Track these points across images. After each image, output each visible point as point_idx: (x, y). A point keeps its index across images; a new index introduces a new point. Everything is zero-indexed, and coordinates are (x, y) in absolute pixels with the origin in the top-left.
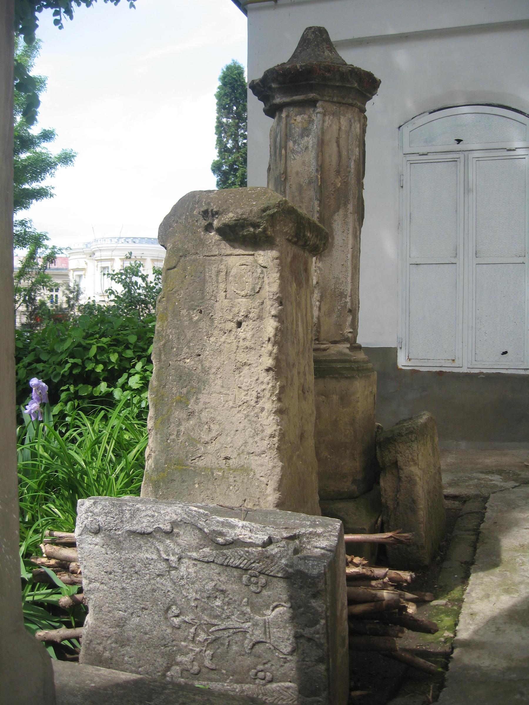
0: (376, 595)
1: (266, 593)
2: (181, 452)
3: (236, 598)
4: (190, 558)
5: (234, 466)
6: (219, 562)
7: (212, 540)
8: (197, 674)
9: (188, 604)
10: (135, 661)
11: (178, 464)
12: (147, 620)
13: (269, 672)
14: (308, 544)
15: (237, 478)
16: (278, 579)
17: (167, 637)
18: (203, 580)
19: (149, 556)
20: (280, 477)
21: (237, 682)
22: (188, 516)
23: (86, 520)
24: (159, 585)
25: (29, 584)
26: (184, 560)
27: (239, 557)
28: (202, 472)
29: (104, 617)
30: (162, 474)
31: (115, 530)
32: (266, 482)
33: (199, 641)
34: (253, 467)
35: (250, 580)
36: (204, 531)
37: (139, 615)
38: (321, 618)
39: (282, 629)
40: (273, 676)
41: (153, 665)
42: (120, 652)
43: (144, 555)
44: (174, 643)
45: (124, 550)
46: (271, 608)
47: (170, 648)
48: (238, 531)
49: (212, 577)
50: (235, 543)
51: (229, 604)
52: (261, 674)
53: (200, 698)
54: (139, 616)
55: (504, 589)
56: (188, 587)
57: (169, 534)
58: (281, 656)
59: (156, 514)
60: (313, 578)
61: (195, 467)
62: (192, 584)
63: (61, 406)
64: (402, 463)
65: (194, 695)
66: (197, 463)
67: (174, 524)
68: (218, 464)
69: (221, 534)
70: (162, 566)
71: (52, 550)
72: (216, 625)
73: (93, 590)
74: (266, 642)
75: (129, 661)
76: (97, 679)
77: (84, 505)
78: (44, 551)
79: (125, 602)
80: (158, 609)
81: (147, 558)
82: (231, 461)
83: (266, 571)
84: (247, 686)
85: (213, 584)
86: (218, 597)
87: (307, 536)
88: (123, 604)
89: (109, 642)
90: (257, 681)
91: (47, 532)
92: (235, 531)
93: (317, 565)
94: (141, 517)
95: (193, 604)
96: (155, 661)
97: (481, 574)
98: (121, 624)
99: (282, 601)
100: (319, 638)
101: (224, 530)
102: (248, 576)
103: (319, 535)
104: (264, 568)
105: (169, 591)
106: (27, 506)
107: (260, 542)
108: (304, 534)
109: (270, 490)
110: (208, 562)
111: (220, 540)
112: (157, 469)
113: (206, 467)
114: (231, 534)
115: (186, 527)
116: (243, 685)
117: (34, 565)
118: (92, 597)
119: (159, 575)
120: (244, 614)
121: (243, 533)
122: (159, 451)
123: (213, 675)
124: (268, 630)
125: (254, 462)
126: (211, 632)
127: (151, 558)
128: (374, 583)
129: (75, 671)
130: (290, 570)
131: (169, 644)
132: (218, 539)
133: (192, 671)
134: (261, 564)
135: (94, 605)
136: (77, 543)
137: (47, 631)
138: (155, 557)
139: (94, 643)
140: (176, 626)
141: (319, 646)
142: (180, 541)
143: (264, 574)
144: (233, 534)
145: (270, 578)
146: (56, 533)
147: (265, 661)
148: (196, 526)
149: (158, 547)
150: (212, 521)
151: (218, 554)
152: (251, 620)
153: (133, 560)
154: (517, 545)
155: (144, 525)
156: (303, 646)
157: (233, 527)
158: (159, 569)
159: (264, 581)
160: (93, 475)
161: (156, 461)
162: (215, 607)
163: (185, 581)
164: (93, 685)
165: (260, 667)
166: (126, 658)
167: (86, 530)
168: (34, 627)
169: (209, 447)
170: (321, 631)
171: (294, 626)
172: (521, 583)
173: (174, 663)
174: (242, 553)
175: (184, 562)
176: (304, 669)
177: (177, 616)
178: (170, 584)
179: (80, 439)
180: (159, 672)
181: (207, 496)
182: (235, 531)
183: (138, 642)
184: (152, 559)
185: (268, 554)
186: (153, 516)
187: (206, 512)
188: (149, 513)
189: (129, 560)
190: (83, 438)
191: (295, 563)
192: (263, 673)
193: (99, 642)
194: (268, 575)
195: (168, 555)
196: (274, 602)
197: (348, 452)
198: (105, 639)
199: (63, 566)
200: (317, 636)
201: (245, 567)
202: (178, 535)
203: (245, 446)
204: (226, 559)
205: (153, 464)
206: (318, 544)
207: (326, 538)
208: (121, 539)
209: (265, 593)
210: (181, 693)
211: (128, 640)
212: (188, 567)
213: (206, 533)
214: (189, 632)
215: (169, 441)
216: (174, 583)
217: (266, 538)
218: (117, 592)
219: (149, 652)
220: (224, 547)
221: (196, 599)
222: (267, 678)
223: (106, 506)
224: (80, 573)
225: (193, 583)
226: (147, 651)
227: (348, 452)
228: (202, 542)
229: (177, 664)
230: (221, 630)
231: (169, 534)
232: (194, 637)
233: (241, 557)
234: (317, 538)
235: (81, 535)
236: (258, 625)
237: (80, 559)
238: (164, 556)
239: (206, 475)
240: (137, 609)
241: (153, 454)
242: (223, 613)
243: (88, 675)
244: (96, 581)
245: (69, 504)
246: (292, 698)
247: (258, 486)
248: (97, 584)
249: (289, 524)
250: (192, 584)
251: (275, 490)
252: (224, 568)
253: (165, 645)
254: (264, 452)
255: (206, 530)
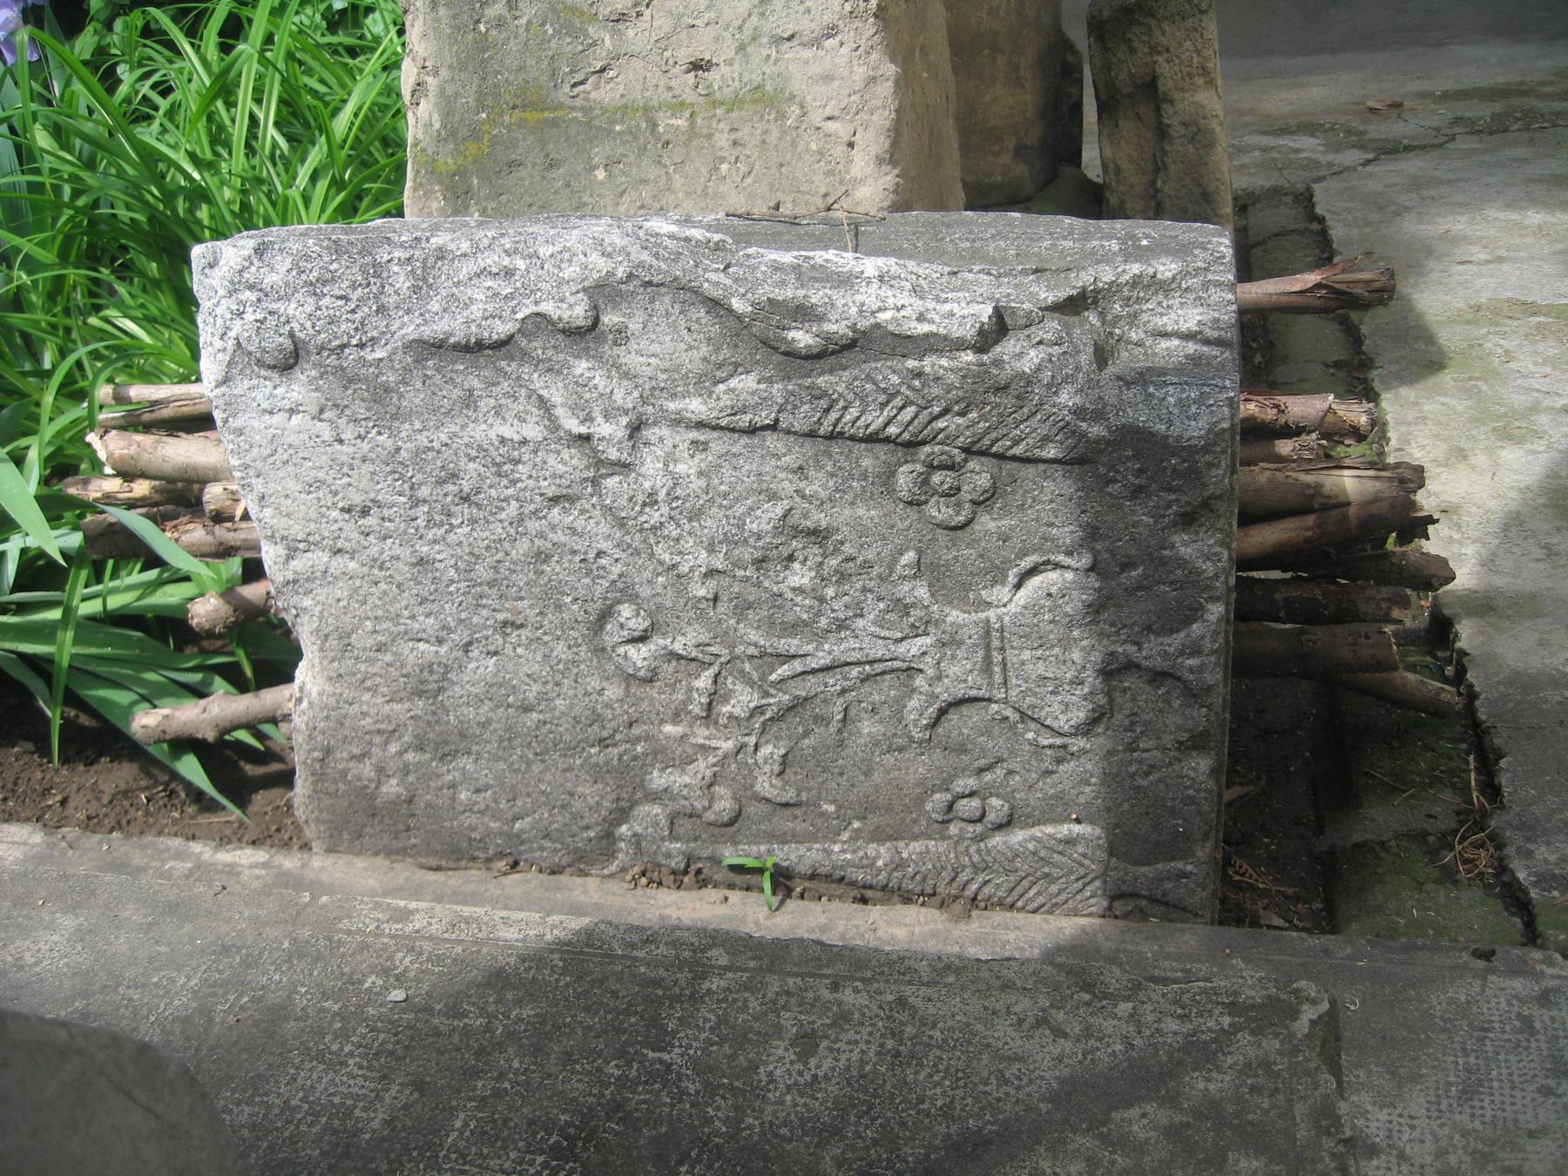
0: (1318, 486)
1: (992, 526)
2: (531, 62)
3: (870, 554)
4: (677, 421)
5: (726, 91)
6: (797, 427)
7: (765, 343)
8: (731, 823)
9: (682, 592)
10: (496, 801)
11: (524, 107)
12: (524, 663)
13: (998, 796)
14: (1131, 325)
15: (744, 133)
16: (1041, 467)
17: (609, 714)
18: (737, 500)
19: (508, 433)
20: (893, 116)
21: (878, 836)
22: (657, 256)
23: (238, 322)
24: (559, 537)
25: (80, 568)
26: (650, 434)
27: (882, 398)
28: (612, 122)
29: (363, 667)
30: (472, 147)
31: (361, 346)
32: (846, 138)
33: (731, 717)
34: (797, 86)
35: (926, 482)
36: (730, 311)
37: (492, 648)
38: (1212, 599)
39: (1056, 650)
40: (1012, 808)
41: (563, 807)
42: (439, 776)
43: (488, 430)
44: (636, 731)
45: (408, 417)
46: (1012, 579)
47: (622, 749)
48: (869, 296)
49: (774, 484)
50: (863, 343)
51: (843, 577)
52: (968, 806)
53: (863, 1000)
54: (496, 653)
55: (1494, 429)
56: (675, 534)
57: (584, 335)
58: (1046, 742)
59: (521, 264)
60: (1189, 452)
61: (586, 110)
62: (690, 520)
63: (96, 33)
64: (1171, 83)
65: (835, 987)
66: (593, 95)
67: (602, 293)
68: (670, 88)
69: (803, 313)
70: (567, 464)
71: (133, 451)
72: (794, 657)
73: (307, 580)
74: (989, 700)
75: (476, 803)
76: (403, 961)
77: (217, 266)
78: (102, 455)
79: (435, 607)
80: (563, 622)
81: (503, 441)
82: (713, 76)
83: (997, 440)
84: (916, 846)
85: (779, 511)
86: (800, 555)
87: (1126, 293)
88: (428, 615)
89: (393, 748)
90: (953, 829)
91: (104, 392)
92: (859, 298)
93: (1200, 401)
94: (457, 284)
95: (702, 592)
96: (572, 794)
97: (1407, 393)
98: (429, 685)
99: (1057, 549)
100: (1201, 669)
101: (816, 296)
102: (919, 468)
103: (1165, 287)
104: (987, 431)
105: (600, 554)
106: (37, 322)
107: (968, 331)
108: (1113, 289)
109: (862, 163)
110: (752, 430)
111: (802, 338)
112: (452, 132)
113: (626, 107)
114: (845, 312)
115: (652, 301)
116: (901, 844)
117: (85, 506)
118: (307, 602)
119: (555, 500)
120: (902, 607)
121: (891, 301)
122: (450, 67)
123: (783, 822)
124: (997, 657)
125: (800, 66)
126: (774, 684)
127: (517, 438)
128: (1285, 447)
129: (306, 933)
130: (1096, 430)
131: (618, 737)
132: (791, 334)
133: (710, 816)
134: (973, 415)
135: (318, 631)
136: (218, 415)
137: (166, 711)
138: (533, 431)
139: (338, 755)
140: (642, 673)
141: (1194, 694)
142: (630, 358)
143: (983, 453)
144: (854, 310)
145: (1009, 465)
146: (140, 392)
147: (982, 762)
148: (696, 292)
149: (544, 393)
150: (754, 268)
151: (792, 393)
152: (932, 630)
153: (447, 453)
154: (1462, 305)
155: (476, 311)
156: (1133, 700)
157: (845, 281)
158: (554, 476)
159: (984, 481)
160: (228, 203)
161: (447, 106)
162: (789, 595)
163: (665, 510)
164: (398, 995)
165: (965, 783)
166: (463, 796)
167: (242, 359)
168: (122, 697)
169: (631, 33)
170: (1208, 645)
171: (1102, 635)
172: (1535, 409)
173: (639, 795)
174: (895, 379)
175: (653, 439)
176: (1132, 776)
177: (643, 639)
178: (604, 528)
179: (164, 104)
180: (588, 828)
181: (642, 207)
182: (859, 298)
183: (501, 740)
184: (524, 442)
185: (1004, 376)
186: (509, 273)
187: (717, 237)
188: (492, 260)
189: (431, 455)
190: (171, 98)
191: (1113, 401)
192: (976, 802)
193: (356, 751)
194: (1001, 457)
195: (589, 419)
196: (1023, 554)
197: (1001, 61)
198: (378, 739)
199: (180, 497)
200: (1191, 662)
201: (906, 436)
202: (621, 335)
203: (763, 14)
204: (827, 410)
205: (436, 117)
206: (1167, 322)
207: (1191, 296)
208: (391, 378)
209: (987, 523)
210: (774, 984)
211: (463, 736)
212: (670, 458)
213: (739, 318)
214: (690, 689)
215: (482, 28)
216: (621, 523)
217: (986, 312)
218: (399, 578)
219: (547, 769)
220: (818, 365)
221: (711, 573)
222: (991, 817)
223: (307, 257)
224: (246, 516)
225: (696, 515)
226: (537, 768)
227: (1001, 61)
228: (725, 353)
229: (654, 797)
230: (813, 672)
231: (584, 335)
232: (710, 704)
233: (892, 396)
234: (1160, 297)
235: (226, 381)
236: (960, 643)
237: (237, 474)
238: (574, 426)
239: (633, 133)
240: (485, 627)
241: (429, 79)
242: (819, 614)
243: (365, 947)
244: (310, 544)
245: (167, 301)
246: (1082, 871)
247: (821, 153)
248: (320, 558)
249: (1038, 255)
250: (690, 520)
251: (880, 161)
252: (821, 445)
253: (601, 741)
254: (831, 31)
255: (737, 304)
